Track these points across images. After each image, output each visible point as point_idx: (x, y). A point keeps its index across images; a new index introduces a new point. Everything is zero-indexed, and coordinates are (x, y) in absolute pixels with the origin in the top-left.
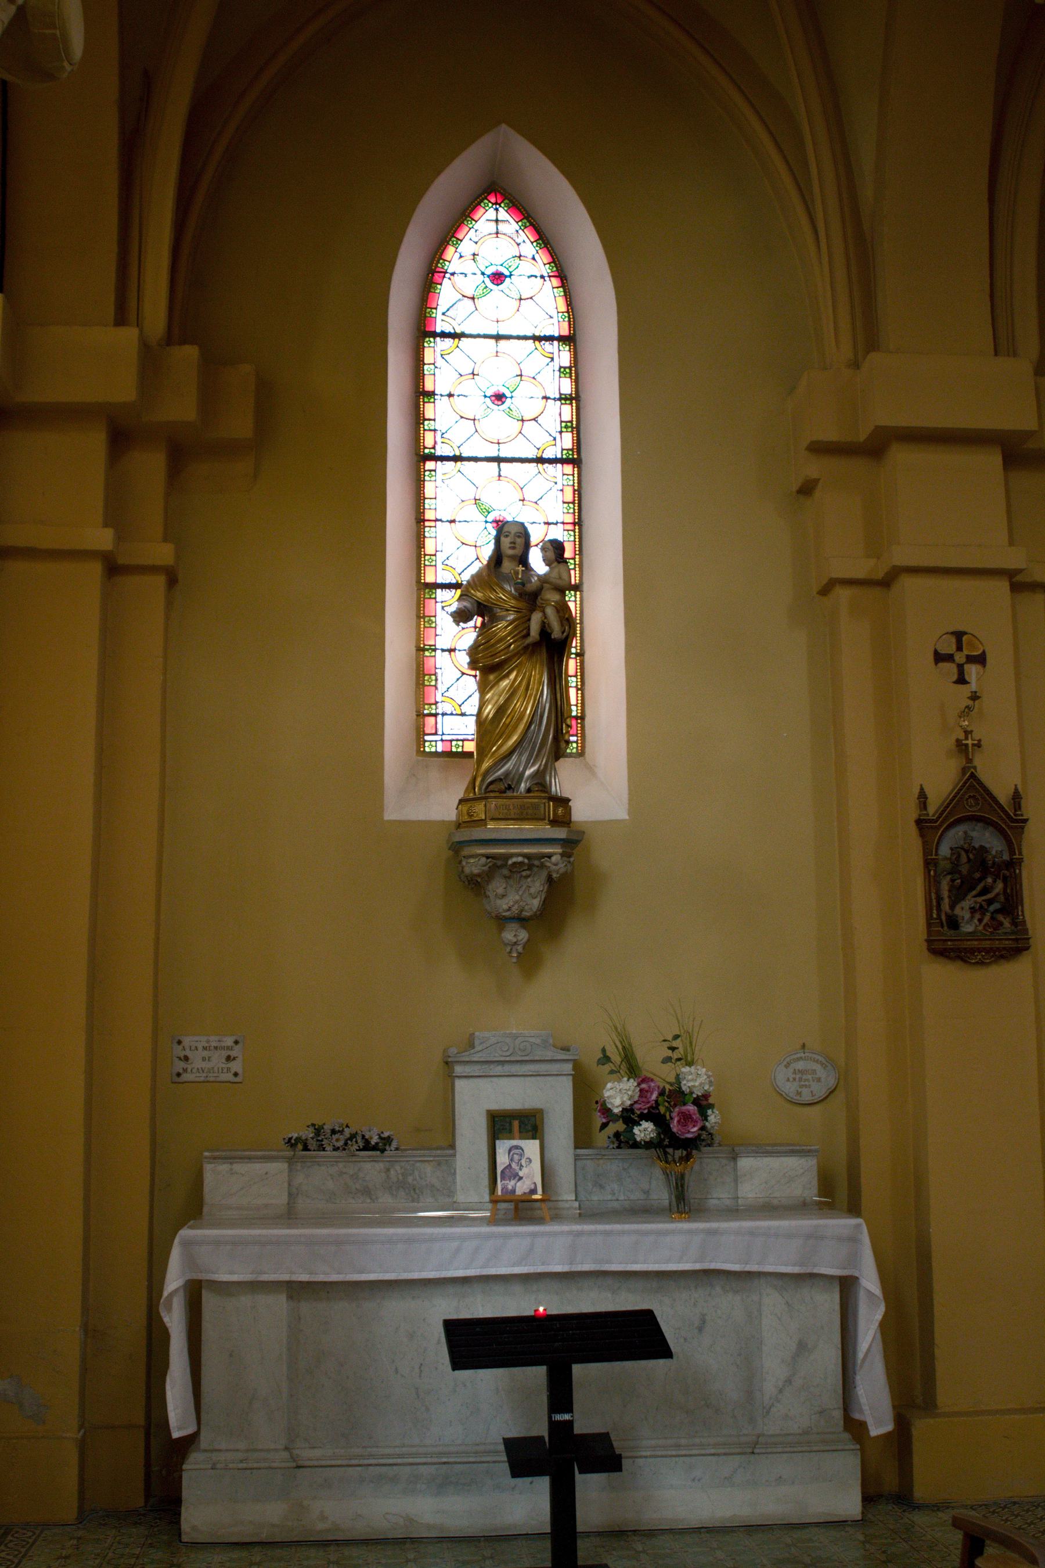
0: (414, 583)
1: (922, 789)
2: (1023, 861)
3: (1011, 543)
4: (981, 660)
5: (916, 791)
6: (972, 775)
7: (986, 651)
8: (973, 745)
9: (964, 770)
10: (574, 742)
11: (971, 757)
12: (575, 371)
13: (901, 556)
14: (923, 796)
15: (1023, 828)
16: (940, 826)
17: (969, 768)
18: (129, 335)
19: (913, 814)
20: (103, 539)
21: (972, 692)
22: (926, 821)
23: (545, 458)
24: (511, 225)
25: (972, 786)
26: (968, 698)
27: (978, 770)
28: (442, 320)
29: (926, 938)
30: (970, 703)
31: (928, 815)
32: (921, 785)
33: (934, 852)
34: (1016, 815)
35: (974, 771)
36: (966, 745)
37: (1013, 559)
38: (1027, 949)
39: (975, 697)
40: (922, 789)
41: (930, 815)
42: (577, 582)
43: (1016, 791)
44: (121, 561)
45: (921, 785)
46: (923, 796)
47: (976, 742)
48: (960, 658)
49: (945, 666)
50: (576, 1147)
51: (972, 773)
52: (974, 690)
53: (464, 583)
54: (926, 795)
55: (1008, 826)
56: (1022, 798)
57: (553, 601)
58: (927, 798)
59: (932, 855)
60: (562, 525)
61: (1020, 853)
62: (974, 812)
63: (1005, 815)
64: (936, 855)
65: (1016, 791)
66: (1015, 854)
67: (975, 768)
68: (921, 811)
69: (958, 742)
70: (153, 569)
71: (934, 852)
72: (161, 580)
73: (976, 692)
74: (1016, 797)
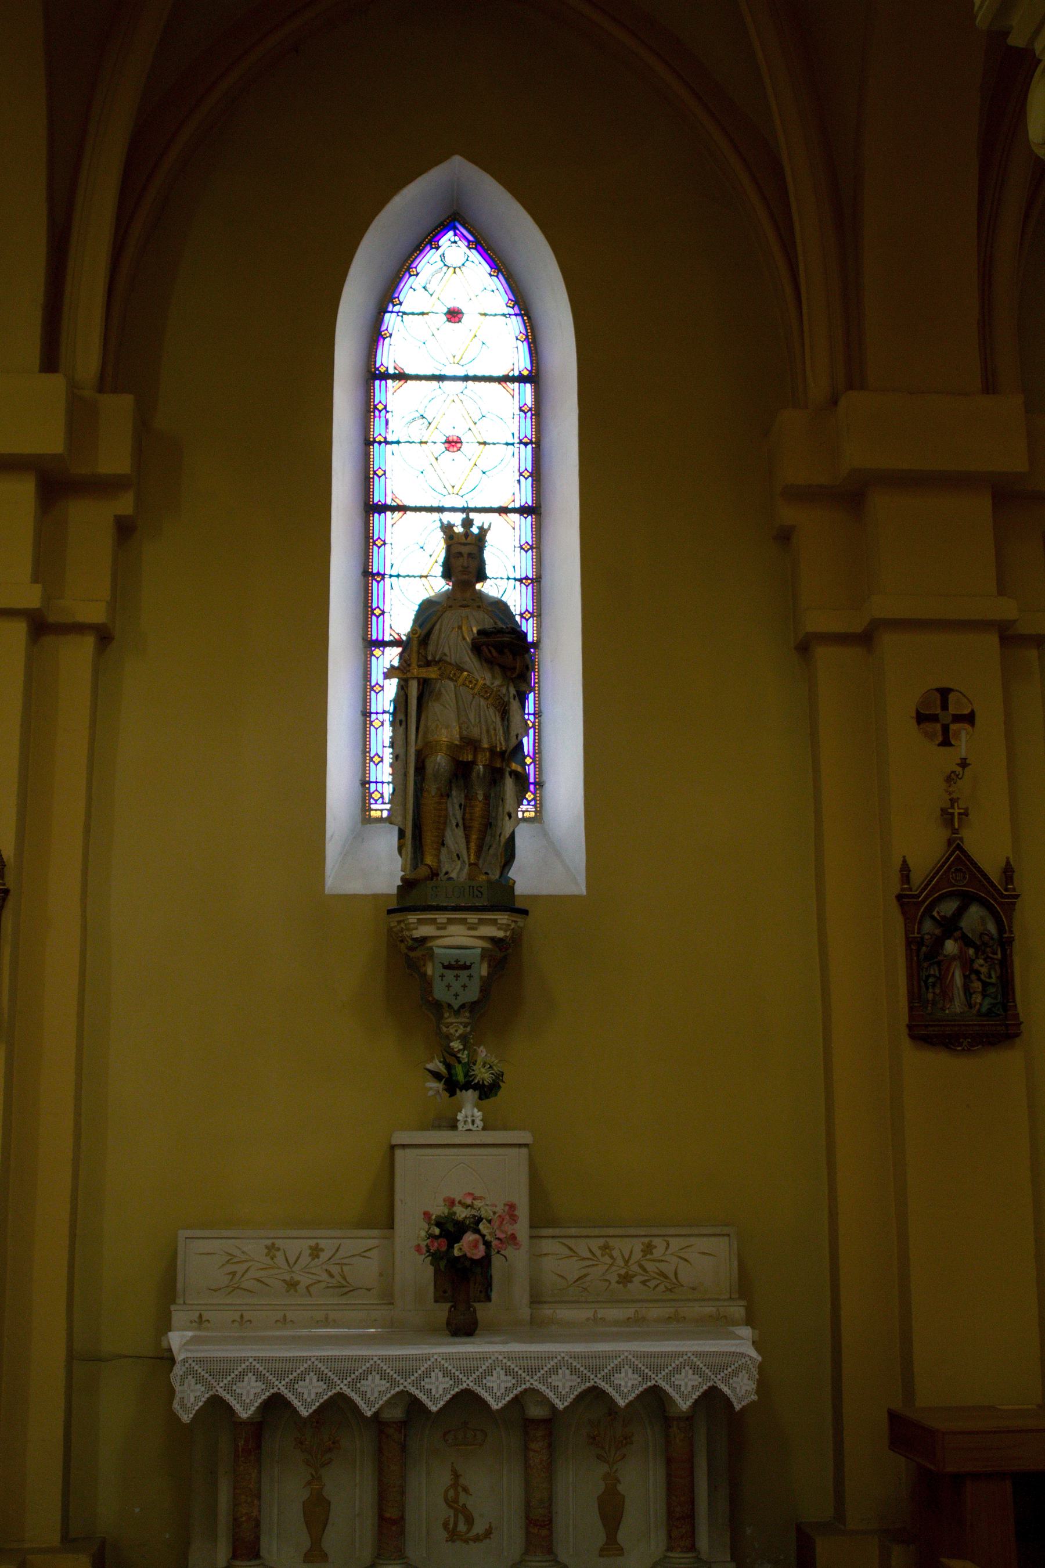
0: (360, 641)
1: (904, 861)
2: (1014, 940)
3: (1001, 592)
4: (970, 719)
5: (897, 864)
6: (959, 847)
7: (975, 710)
8: (960, 814)
9: (950, 842)
10: (523, 814)
11: (956, 826)
12: (537, 412)
13: (882, 607)
14: (905, 871)
15: (1014, 904)
16: (924, 901)
17: (956, 839)
18: (56, 382)
19: (896, 888)
20: (31, 598)
21: (961, 759)
22: (908, 896)
23: (518, 513)
24: (478, 268)
25: (958, 858)
26: (958, 764)
27: (965, 843)
28: (513, 434)
29: (907, 1022)
30: (959, 769)
31: (910, 889)
32: (904, 857)
33: (916, 931)
34: (1006, 890)
35: (960, 843)
36: (952, 814)
37: (1006, 609)
38: (1017, 1035)
39: (964, 764)
40: (904, 861)
41: (914, 888)
42: (535, 639)
43: (1008, 863)
44: (51, 619)
45: (904, 857)
46: (905, 871)
47: (962, 811)
48: (945, 718)
49: (929, 727)
50: (531, 1227)
51: (958, 844)
52: (963, 757)
53: (404, 638)
54: (909, 868)
55: (997, 903)
56: (1014, 872)
57: (535, 652)
58: (910, 871)
59: (914, 934)
60: (513, 581)
61: (1011, 932)
62: (960, 886)
63: (982, 875)
64: (918, 933)
65: (1008, 863)
66: (1005, 933)
67: (961, 839)
68: (903, 884)
69: (944, 811)
70: (80, 628)
71: (916, 931)
72: (89, 642)
73: (965, 759)
74: (1008, 872)
